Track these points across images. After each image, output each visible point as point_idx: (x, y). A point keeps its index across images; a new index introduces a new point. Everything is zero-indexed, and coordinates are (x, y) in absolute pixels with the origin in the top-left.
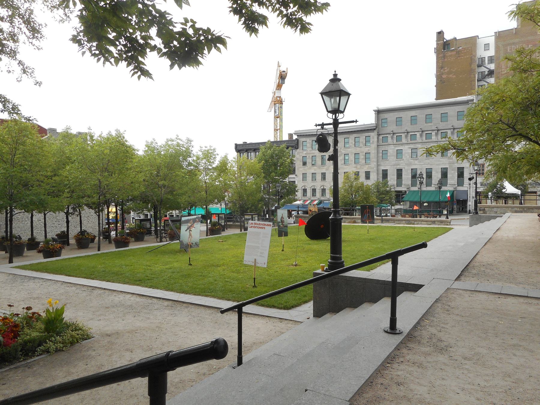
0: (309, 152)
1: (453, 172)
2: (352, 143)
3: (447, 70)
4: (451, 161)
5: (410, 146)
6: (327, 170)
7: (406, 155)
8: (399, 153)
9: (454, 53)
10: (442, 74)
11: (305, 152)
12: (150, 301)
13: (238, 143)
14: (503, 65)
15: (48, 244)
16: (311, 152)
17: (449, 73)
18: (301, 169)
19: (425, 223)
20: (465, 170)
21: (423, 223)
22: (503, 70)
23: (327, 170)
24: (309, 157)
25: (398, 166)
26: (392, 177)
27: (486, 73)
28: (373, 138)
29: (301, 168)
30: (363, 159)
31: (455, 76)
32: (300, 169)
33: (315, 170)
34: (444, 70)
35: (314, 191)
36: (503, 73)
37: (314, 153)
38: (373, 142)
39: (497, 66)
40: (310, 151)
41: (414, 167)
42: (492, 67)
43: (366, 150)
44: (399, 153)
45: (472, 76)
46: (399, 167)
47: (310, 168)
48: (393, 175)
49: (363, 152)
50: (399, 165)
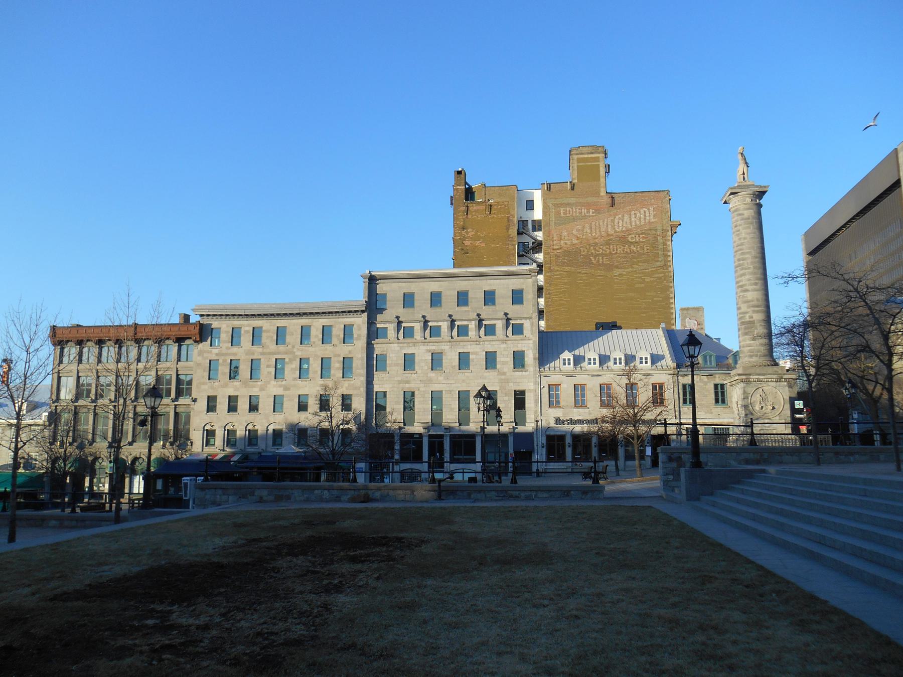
0: (224, 351)
1: (506, 398)
2: (316, 336)
3: (471, 232)
4: (503, 377)
5: (428, 348)
6: (262, 389)
7: (423, 364)
8: (409, 362)
9: (483, 207)
10: (464, 238)
11: (215, 351)
12: (494, 317)
13: (59, 324)
14: (555, 234)
15: (133, 503)
16: (230, 351)
17: (475, 238)
18: (206, 387)
19: (545, 495)
20: (527, 395)
21: (540, 495)
22: (555, 242)
23: (262, 389)
24: (224, 361)
25: (407, 386)
26: (395, 406)
27: (531, 245)
28: (360, 329)
29: (204, 384)
30: (338, 369)
31: (483, 245)
32: (203, 387)
33: (236, 389)
34: (467, 233)
35: (278, 373)
36: (555, 247)
37: (235, 354)
38: (359, 336)
39: (548, 235)
40: (227, 348)
41: (436, 387)
42: (539, 235)
43: (345, 350)
44: (409, 362)
45: (511, 247)
46: (407, 387)
47: (226, 386)
48: (397, 403)
49: (339, 356)
50: (408, 382)
